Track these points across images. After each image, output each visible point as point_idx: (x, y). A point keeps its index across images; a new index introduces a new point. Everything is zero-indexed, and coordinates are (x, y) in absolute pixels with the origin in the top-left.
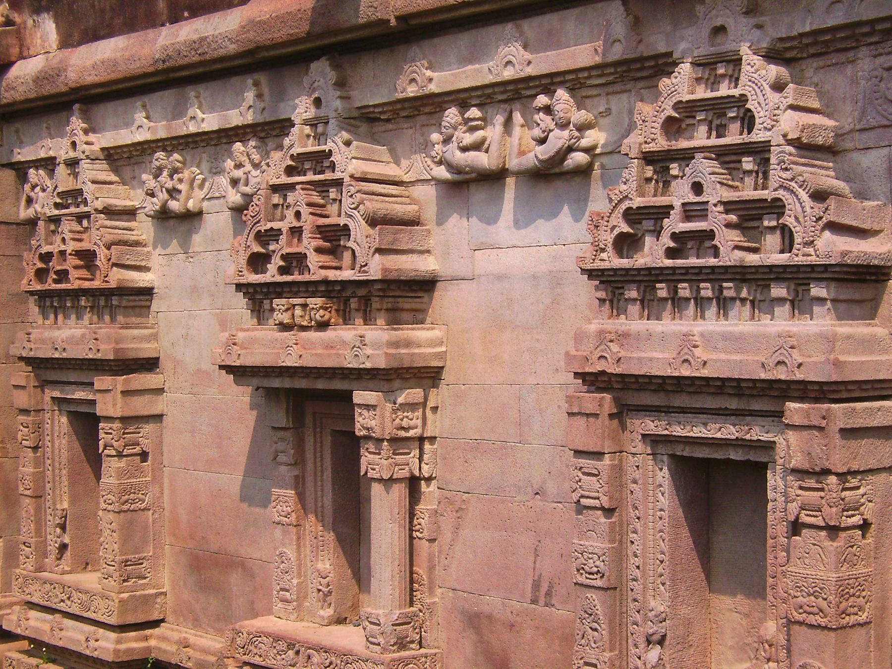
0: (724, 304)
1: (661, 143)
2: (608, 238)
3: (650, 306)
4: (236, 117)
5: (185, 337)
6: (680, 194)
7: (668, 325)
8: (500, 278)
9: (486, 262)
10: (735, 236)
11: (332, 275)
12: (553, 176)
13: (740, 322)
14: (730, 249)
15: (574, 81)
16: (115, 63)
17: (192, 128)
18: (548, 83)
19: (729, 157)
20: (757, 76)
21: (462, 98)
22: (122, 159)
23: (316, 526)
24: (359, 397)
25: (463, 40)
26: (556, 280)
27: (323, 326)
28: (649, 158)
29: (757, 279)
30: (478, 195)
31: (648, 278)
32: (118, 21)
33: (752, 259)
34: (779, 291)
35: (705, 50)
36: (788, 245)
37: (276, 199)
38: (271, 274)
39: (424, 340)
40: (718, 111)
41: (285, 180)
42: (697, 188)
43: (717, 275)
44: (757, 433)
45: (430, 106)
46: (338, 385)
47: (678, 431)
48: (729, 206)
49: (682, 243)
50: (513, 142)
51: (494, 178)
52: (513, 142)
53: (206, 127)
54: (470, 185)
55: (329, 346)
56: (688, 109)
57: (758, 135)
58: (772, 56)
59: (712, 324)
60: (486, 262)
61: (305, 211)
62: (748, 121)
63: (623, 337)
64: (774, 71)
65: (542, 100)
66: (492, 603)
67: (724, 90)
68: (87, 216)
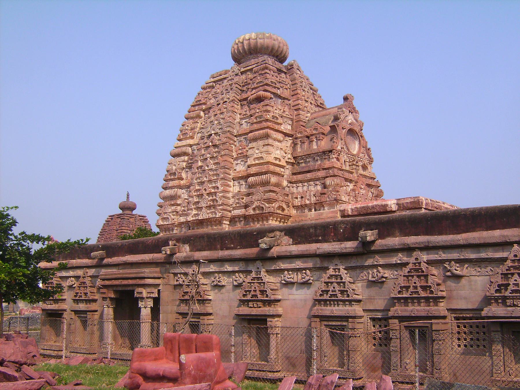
0: (346, 305)
1: (327, 280)
2: (318, 294)
3: (325, 305)
4: (236, 269)
5: (220, 309)
6: (331, 288)
7: (329, 308)
8: (294, 300)
9: (291, 297)
10: (340, 295)
11: (262, 298)
12: (306, 284)
13: (341, 307)
14: (340, 297)
15: (310, 269)
16: (207, 256)
17: (226, 270)
18: (305, 269)
19: (339, 283)
20: (343, 272)
21: (288, 270)
22: (206, 274)
23: (75, 328)
24: (268, 320)
25: (289, 260)
26: (305, 300)
27: (260, 307)
28: (325, 283)
29: (344, 301)
30: (290, 286)
31: (325, 301)
32: (207, 248)
33: (343, 298)
34: (347, 303)
35: (256, 270)
36: (201, 297)
37: (249, 285)
38: (77, 298)
39: (280, 310)
40: (258, 278)
41: (251, 281)
42: (334, 288)
43: (338, 301)
44: (344, 323)
45: (282, 271)
46: (265, 318)
47: (330, 323)
48: (339, 291)
49: (253, 296)
50: (297, 277)
51: (293, 283)
52: (297, 277)
53: (229, 270)
54: (288, 284)
55: (262, 311)
56: (332, 276)
57: (343, 281)
58: (344, 269)
59: (336, 308)
60: (291, 297)
61: (257, 287)
62: (342, 278)
63: (321, 310)
64: (346, 271)
65: (304, 271)
66: (291, 354)
67: (259, 276)
68: (87, 287)
